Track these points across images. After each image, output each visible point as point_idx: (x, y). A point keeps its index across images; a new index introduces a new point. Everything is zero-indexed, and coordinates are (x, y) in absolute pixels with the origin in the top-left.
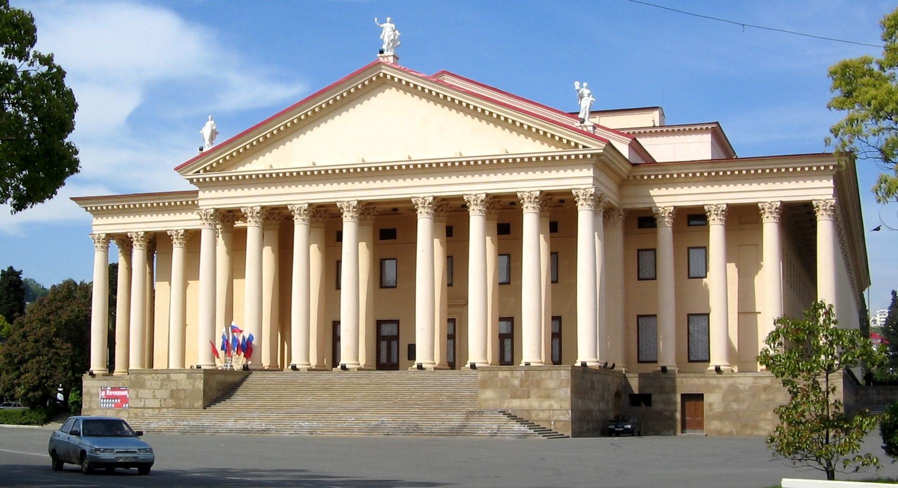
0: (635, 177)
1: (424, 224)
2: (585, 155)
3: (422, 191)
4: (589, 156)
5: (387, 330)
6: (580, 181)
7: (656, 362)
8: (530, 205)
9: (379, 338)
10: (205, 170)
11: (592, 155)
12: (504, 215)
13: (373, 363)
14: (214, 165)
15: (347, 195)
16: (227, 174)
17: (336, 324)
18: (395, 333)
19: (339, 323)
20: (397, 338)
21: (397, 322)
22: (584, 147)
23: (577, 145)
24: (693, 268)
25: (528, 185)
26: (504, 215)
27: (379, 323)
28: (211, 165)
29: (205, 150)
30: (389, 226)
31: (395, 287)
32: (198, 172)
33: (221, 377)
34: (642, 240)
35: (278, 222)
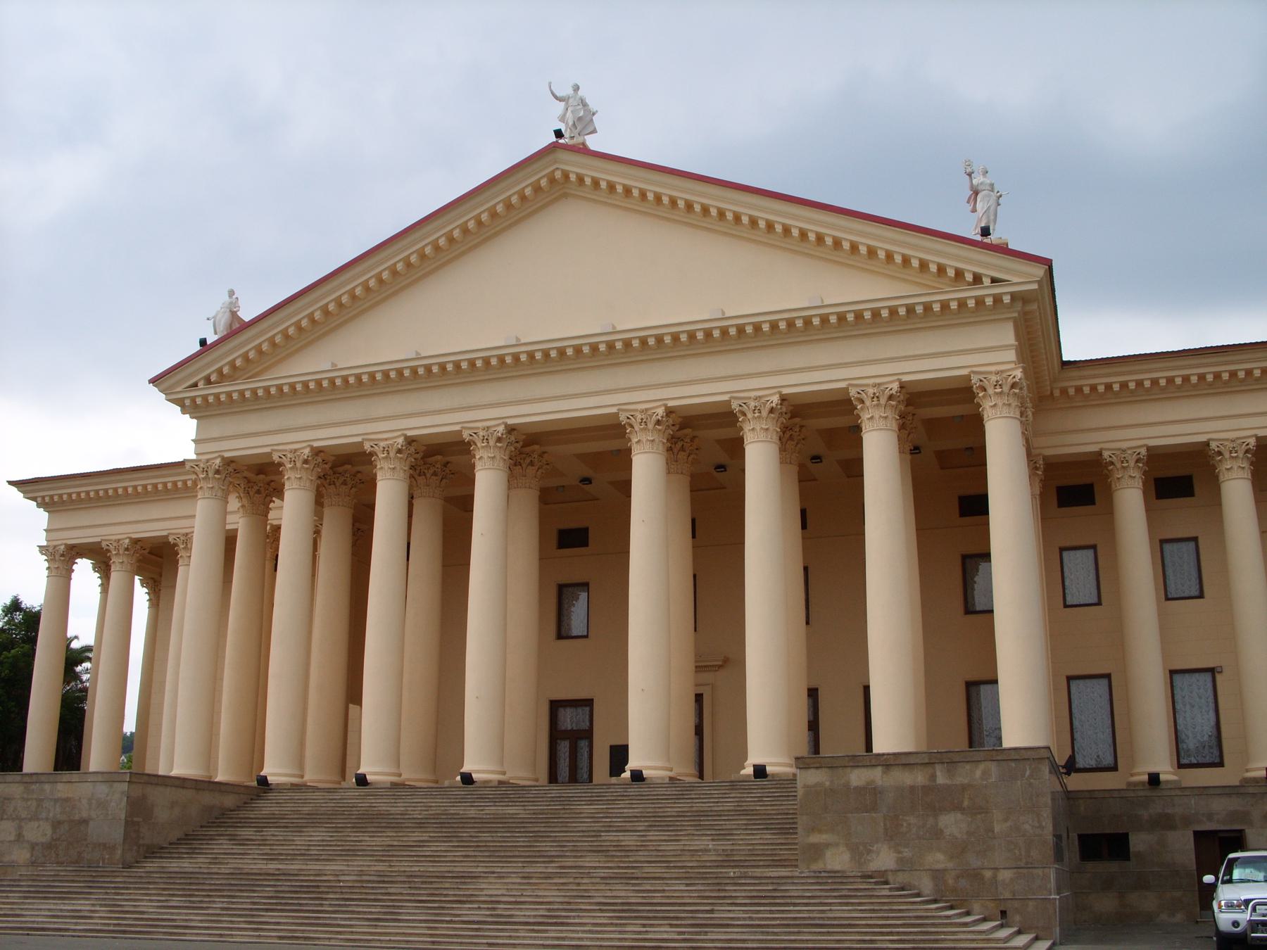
0: (1064, 391)
1: (647, 473)
2: (997, 299)
4: (1007, 299)
5: (569, 720)
6: (987, 354)
8: (877, 413)
9: (555, 734)
10: (208, 381)
11: (1014, 296)
12: (821, 443)
14: (226, 370)
18: (585, 726)
20: (588, 734)
21: (588, 703)
22: (994, 280)
23: (977, 279)
25: (871, 371)
26: (821, 443)
27: (556, 706)
28: (220, 371)
31: (586, 637)
32: (195, 385)
33: (208, 799)
34: (1182, 517)
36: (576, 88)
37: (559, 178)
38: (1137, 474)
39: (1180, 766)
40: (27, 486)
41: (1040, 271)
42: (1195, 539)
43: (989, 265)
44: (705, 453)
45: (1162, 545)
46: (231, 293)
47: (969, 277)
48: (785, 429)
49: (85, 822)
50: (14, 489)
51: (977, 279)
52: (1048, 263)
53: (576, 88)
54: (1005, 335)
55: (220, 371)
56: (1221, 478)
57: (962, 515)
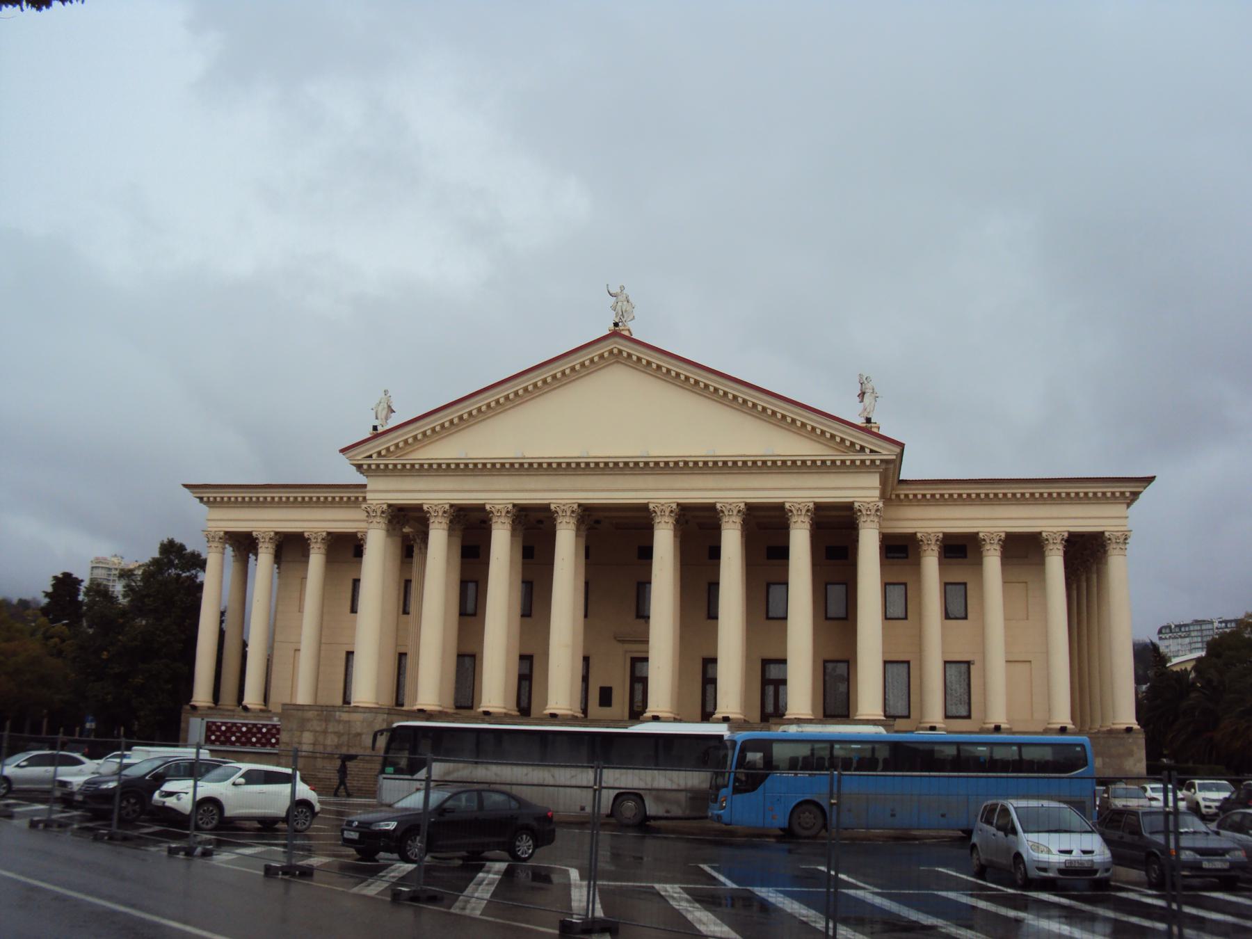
0: (898, 496)
1: (664, 541)
2: (873, 461)
3: (663, 495)
4: (878, 463)
5: (774, 672)
6: (861, 490)
7: (471, 708)
9: (765, 682)
11: (882, 461)
12: (765, 528)
13: (820, 715)
15: (563, 495)
16: (390, 461)
17: (710, 662)
19: (714, 661)
22: (872, 451)
24: (958, 605)
25: (800, 494)
26: (765, 528)
28: (388, 449)
29: (380, 429)
30: (617, 539)
32: (370, 456)
35: (471, 528)
36: (622, 288)
37: (618, 349)
38: (936, 548)
39: (947, 717)
40: (1153, 478)
41: (898, 450)
42: (965, 584)
43: (869, 442)
44: (699, 527)
45: (946, 586)
46: (386, 392)
47: (858, 447)
48: (390, 522)
49: (359, 735)
50: (186, 490)
51: (862, 448)
52: (902, 446)
53: (622, 288)
54: (874, 481)
55: (388, 449)
56: (985, 553)
57: (827, 558)
